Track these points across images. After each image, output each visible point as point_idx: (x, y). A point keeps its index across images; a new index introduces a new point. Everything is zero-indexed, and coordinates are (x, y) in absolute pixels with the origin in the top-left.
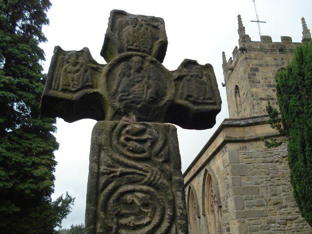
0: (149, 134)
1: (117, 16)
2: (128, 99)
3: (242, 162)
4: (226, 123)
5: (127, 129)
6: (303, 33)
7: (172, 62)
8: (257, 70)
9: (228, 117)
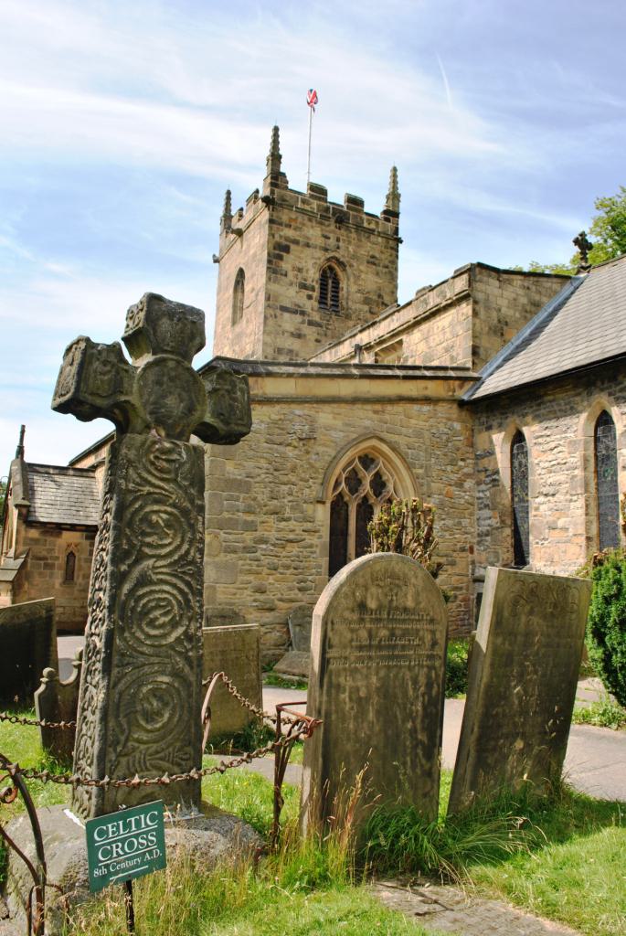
1: (153, 299)
6: (388, 198)
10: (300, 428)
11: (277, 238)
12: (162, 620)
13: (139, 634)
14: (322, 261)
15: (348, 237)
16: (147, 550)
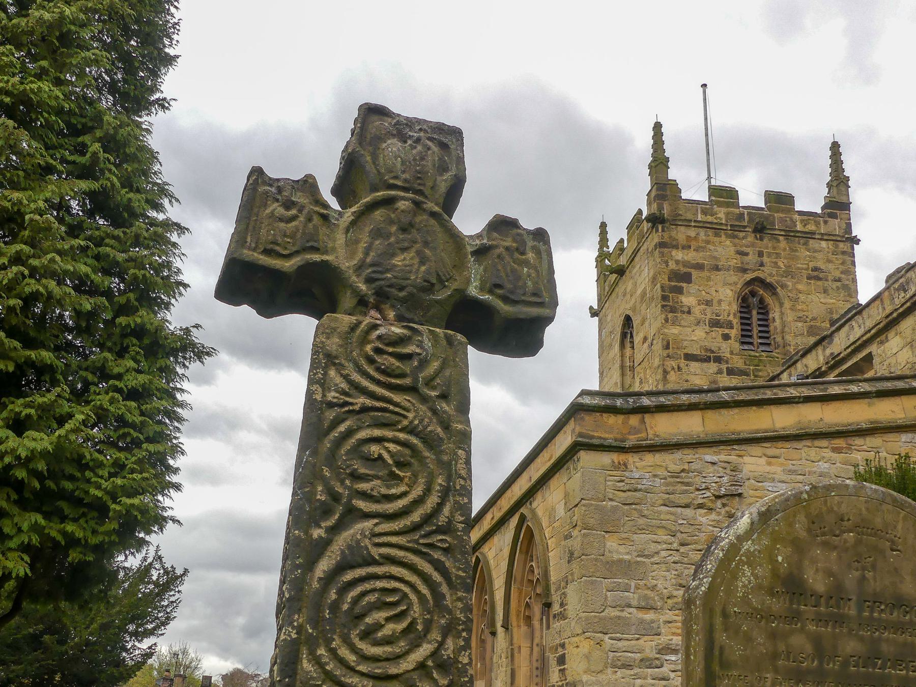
0: (418, 346)
2: (383, 279)
3: (611, 500)
4: (587, 400)
5: (378, 332)
6: (829, 185)
7: (470, 220)
8: (687, 278)
9: (595, 387)
10: (722, 482)
11: (672, 265)
12: (389, 629)
13: (344, 652)
14: (739, 286)
15: (774, 248)
16: (361, 504)
